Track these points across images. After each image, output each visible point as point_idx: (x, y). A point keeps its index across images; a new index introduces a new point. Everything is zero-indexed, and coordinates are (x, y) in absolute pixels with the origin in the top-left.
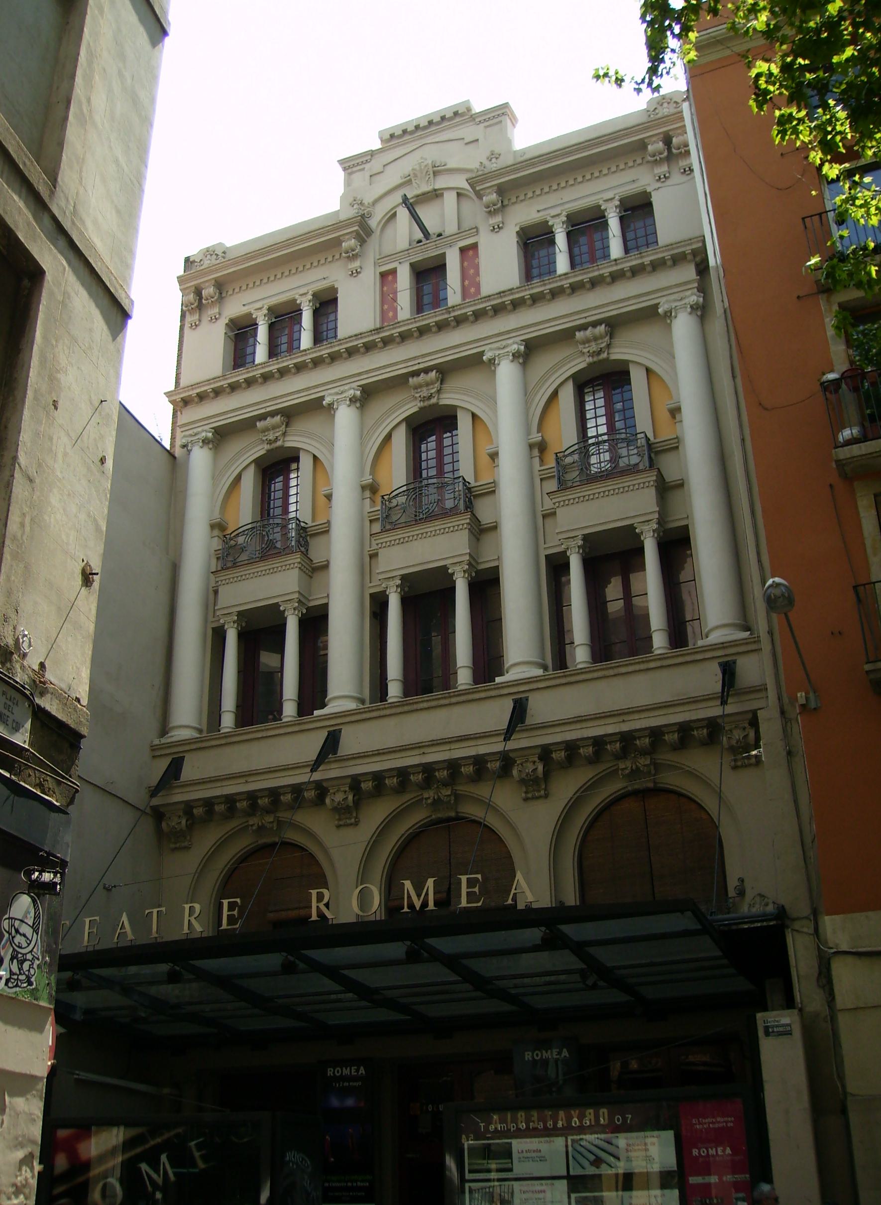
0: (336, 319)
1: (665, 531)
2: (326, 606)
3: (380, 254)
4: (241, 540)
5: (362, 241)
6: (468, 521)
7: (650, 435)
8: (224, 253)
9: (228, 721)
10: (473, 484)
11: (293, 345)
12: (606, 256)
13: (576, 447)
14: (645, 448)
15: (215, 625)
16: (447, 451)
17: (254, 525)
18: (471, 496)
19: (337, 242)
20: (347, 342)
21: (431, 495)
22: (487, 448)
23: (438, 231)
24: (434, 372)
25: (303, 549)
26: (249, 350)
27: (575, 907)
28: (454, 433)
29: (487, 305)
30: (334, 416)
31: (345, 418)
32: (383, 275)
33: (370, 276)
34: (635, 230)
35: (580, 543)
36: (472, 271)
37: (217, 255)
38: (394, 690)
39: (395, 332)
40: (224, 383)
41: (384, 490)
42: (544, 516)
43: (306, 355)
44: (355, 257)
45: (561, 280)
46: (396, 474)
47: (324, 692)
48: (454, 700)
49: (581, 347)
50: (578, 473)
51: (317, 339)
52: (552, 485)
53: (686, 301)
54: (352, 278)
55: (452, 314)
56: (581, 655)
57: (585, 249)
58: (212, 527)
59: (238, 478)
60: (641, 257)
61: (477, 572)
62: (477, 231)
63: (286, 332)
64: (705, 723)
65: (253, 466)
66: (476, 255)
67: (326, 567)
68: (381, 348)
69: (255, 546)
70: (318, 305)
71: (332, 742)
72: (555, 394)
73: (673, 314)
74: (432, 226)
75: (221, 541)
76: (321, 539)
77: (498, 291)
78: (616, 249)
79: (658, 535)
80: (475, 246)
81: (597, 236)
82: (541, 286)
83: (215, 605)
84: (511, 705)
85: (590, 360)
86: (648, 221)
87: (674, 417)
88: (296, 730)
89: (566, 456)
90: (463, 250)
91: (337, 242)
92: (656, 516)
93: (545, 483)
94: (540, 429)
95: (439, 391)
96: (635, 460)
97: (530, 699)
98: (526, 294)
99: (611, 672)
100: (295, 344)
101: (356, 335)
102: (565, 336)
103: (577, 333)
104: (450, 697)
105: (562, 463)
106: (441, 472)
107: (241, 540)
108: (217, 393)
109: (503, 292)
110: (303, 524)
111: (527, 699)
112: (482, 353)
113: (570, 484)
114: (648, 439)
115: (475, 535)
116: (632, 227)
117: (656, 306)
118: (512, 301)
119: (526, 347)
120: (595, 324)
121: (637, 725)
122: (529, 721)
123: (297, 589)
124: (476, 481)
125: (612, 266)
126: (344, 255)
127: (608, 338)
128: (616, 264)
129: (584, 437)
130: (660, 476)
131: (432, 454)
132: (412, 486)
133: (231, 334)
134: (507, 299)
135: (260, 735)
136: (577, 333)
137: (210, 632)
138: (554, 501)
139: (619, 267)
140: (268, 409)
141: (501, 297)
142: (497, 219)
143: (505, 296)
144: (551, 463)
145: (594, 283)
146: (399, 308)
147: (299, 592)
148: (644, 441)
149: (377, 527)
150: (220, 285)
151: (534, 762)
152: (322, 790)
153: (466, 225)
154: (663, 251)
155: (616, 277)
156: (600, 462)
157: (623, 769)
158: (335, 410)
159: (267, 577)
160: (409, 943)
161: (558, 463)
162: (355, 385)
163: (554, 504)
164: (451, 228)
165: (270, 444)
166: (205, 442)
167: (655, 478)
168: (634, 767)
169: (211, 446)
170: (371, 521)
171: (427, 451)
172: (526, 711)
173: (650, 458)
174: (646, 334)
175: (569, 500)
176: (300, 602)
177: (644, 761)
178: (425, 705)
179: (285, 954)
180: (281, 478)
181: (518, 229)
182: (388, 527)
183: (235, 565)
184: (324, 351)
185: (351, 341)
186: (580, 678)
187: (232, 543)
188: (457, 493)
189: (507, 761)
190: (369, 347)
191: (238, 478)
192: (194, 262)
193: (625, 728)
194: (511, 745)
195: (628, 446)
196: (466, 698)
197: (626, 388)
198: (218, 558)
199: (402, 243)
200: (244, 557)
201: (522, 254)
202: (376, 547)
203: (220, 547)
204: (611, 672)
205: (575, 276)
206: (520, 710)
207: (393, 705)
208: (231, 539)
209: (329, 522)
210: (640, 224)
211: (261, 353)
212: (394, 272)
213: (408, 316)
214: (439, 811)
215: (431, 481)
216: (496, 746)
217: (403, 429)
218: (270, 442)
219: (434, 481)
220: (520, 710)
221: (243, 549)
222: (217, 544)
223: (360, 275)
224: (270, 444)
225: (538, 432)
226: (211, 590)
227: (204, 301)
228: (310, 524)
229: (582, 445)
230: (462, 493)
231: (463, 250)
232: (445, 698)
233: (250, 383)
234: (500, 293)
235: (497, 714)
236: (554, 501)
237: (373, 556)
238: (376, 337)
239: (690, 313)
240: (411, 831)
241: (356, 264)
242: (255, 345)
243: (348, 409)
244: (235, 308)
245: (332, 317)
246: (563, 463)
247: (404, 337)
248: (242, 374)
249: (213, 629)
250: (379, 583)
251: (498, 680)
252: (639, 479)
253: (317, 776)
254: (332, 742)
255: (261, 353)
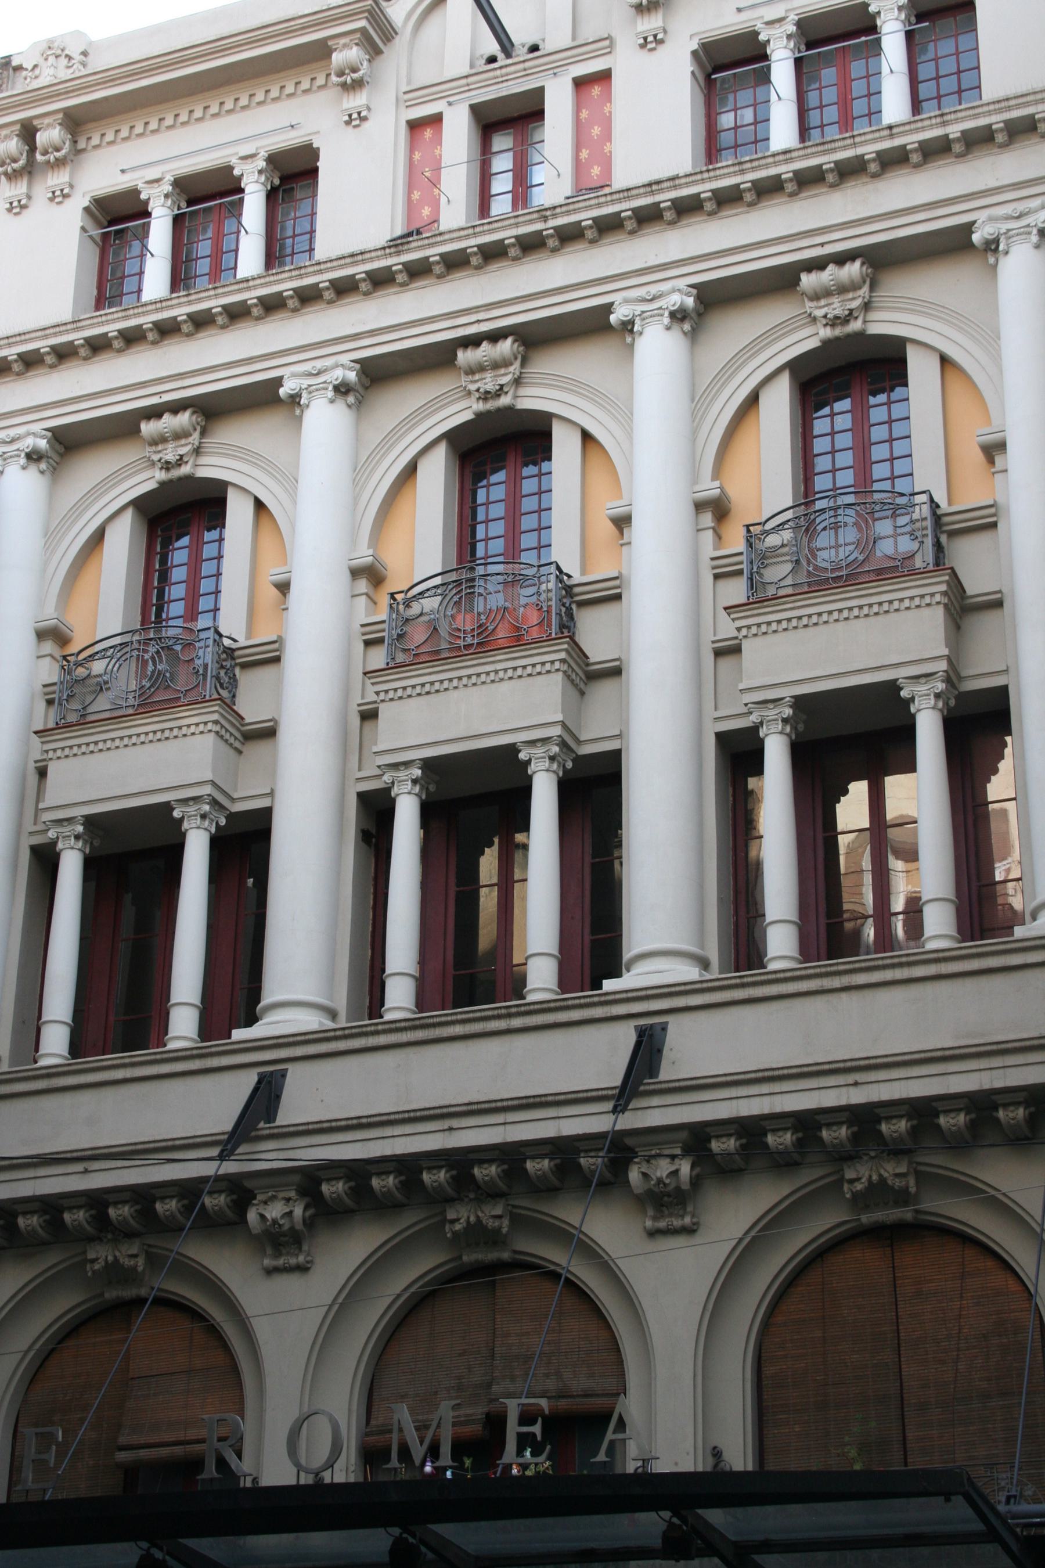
0: (313, 214)
1: (964, 697)
2: (266, 814)
3: (409, 83)
4: (98, 667)
5: (374, 51)
6: (563, 655)
7: (941, 498)
8: (85, 54)
9: (55, 1042)
10: (577, 578)
11: (222, 264)
12: (873, 113)
13: (789, 514)
14: (928, 523)
15: (37, 840)
16: (528, 504)
17: (126, 638)
18: (575, 601)
19: (321, 51)
20: (333, 269)
21: (493, 598)
22: (272, 572)
23: (531, 41)
24: (510, 340)
25: (224, 693)
26: (130, 267)
27: (745, 1473)
28: (545, 466)
29: (624, 207)
30: (300, 419)
31: (658, 348)
32: (415, 126)
33: (387, 126)
34: (936, 59)
35: (788, 712)
36: (596, 131)
37: (69, 57)
38: (399, 996)
39: (433, 253)
40: (77, 337)
41: (397, 582)
42: (718, 653)
43: (248, 289)
44: (358, 85)
45: (776, 164)
46: (423, 546)
47: (255, 992)
48: (517, 1022)
49: (809, 305)
50: (789, 567)
51: (274, 255)
52: (736, 591)
53: (1029, 220)
54: (644, 52)
55: (552, 223)
56: (780, 943)
57: (831, 95)
58: (42, 635)
59: (98, 537)
60: (944, 124)
61: (579, 760)
62: (611, 46)
63: (209, 234)
64: (1021, 1096)
65: (128, 515)
66: (608, 96)
67: (268, 733)
68: (402, 285)
69: (127, 681)
70: (277, 182)
71: (266, 1096)
72: (753, 400)
73: (1001, 247)
74: (520, 35)
75: (56, 667)
76: (988, 620)
77: (646, 180)
78: (894, 102)
79: (946, 704)
80: (604, 77)
81: (857, 68)
82: (735, 173)
83: (38, 802)
84: (632, 1038)
85: (826, 333)
86: (964, 41)
87: (991, 461)
88: (195, 1066)
89: (767, 533)
90: (581, 83)
91: (321, 51)
92: (943, 665)
93: (722, 584)
94: (718, 471)
95: (867, 306)
96: (906, 545)
97: (670, 1026)
98: (704, 188)
99: (836, 982)
100: (227, 260)
101: (352, 255)
102: (782, 281)
103: (804, 277)
104: (510, 1016)
105: (760, 546)
106: (512, 552)
107: (98, 667)
108: (64, 354)
109: (658, 182)
110: (227, 642)
111: (664, 1028)
112: (608, 308)
113: (771, 591)
114: (934, 505)
115: (576, 686)
116: (931, 55)
117: (968, 228)
118: (674, 201)
119: (699, 298)
120: (841, 259)
121: (830, 1099)
122: (667, 1073)
123: (560, 717)
124: (583, 572)
125: (881, 139)
126: (334, 79)
127: (866, 289)
128: (891, 136)
129: (806, 496)
130: (956, 585)
131: (498, 510)
132: (454, 576)
133: (97, 232)
134: (665, 197)
135: (120, 1074)
136: (804, 277)
137: (25, 856)
138: (46, 747)
139: (897, 142)
140: (166, 398)
141: (652, 193)
142: (652, 23)
143: (661, 191)
144: (735, 542)
145: (850, 171)
146: (443, 200)
147: (213, 783)
148: (926, 510)
149: (378, 658)
150: (76, 122)
151: (288, 1200)
152: (241, 1191)
153: (588, 33)
154: (989, 113)
155: (894, 160)
156: (837, 546)
157: (851, 1181)
158: (303, 408)
159: (148, 747)
160: (396, 1531)
161: (750, 545)
162: (345, 359)
163: (739, 629)
164: (558, 38)
165: (168, 469)
166: (342, 389)
167: (943, 588)
168: (875, 1177)
169: (43, 466)
170: (368, 643)
171: (487, 504)
172: (660, 1051)
173: (938, 547)
174: (940, 285)
175: (769, 623)
176: (563, 744)
177: (891, 1170)
178: (458, 1030)
179: (145, 1545)
180: (185, 541)
181: (695, 47)
182: (401, 658)
183: (83, 722)
184: (286, 284)
185: (341, 267)
186: (784, 991)
187: (81, 672)
188: (543, 596)
189: (621, 1149)
190: (381, 280)
191: (98, 537)
192: (19, 68)
193: (857, 1097)
194: (629, 1121)
195: (894, 516)
196: (547, 1020)
197: (898, 392)
198: (50, 702)
199: (457, 65)
200: (102, 704)
201: (701, 99)
202: (374, 698)
203: (55, 679)
204: (836, 982)
205: (806, 157)
206: (648, 1050)
207: (395, 1027)
208: (78, 664)
209: (279, 641)
210: (946, 47)
211: (155, 278)
212: (436, 120)
213: (462, 223)
214: (481, 1224)
215: (491, 569)
216: (594, 1121)
217: (440, 456)
218: (167, 466)
219: (499, 568)
220: (648, 1050)
221: (101, 688)
222: (49, 672)
223: (366, 125)
224: (168, 469)
225: (369, 548)
226: (31, 766)
227: (39, 157)
228: (243, 642)
229: (802, 510)
230: (552, 595)
231: (581, 83)
232: (499, 1017)
233: (132, 338)
234: (650, 185)
235: (599, 1056)
236: (46, 747)
237: (369, 716)
238: (394, 261)
239: (1037, 247)
240: (412, 1290)
241: (357, 101)
242: (142, 256)
243: (332, 406)
244: (106, 171)
245: (304, 207)
246: (760, 546)
247: (455, 263)
248: (114, 321)
249: (362, 796)
250: (379, 772)
251: (609, 985)
252: (910, 589)
253: (230, 1167)
254: (266, 1096)
255: (155, 278)
